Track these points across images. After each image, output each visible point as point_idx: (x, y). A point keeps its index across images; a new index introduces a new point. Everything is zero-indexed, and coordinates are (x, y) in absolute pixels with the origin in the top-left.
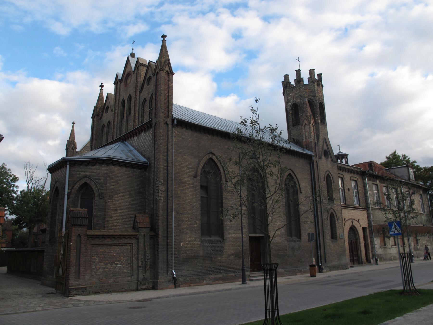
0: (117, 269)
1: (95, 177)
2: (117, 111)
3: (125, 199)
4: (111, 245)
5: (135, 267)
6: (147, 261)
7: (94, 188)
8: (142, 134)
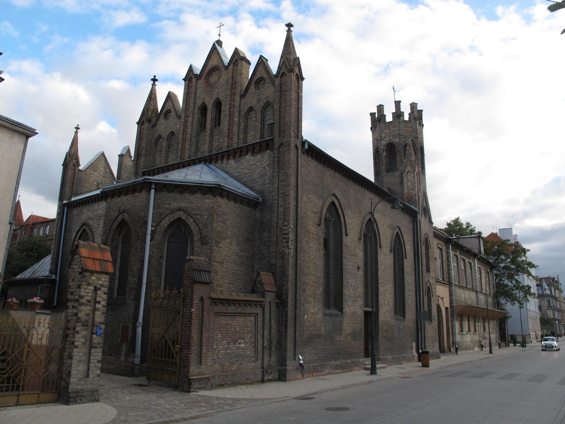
1: (195, 212)
2: (190, 119)
3: (232, 248)
4: (233, 315)
5: (260, 348)
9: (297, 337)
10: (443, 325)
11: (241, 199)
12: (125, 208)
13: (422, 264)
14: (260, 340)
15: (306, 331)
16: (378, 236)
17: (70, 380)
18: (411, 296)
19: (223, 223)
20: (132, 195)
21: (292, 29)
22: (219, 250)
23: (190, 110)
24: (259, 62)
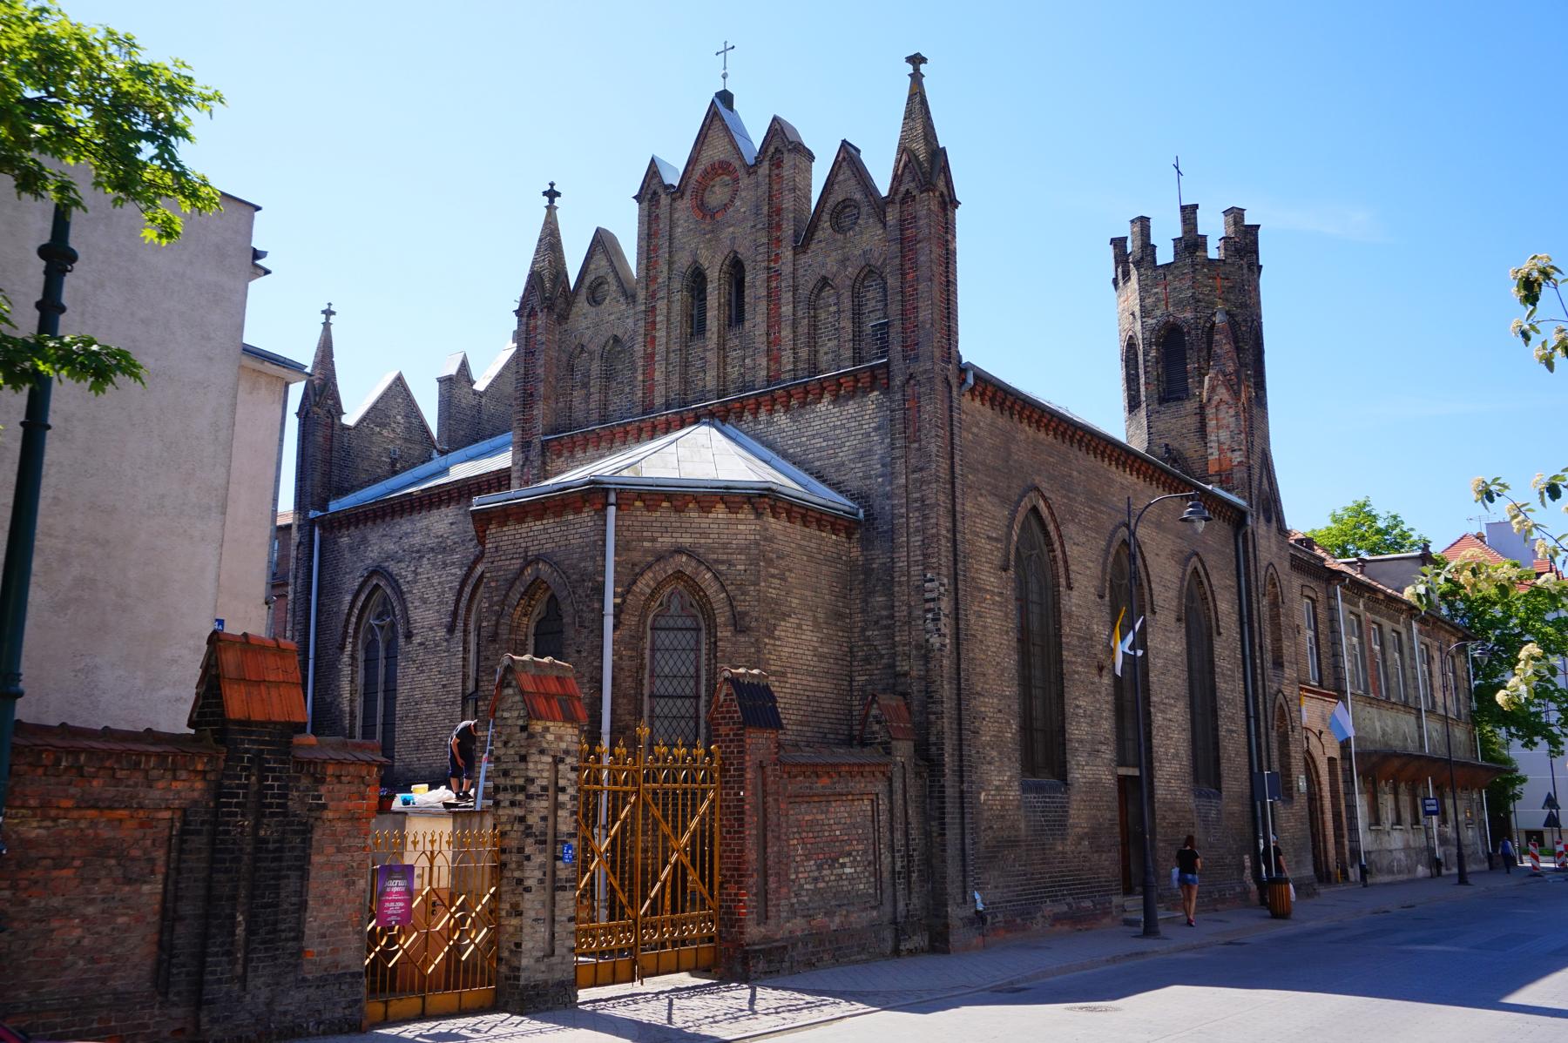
2: (661, 306)
3: (804, 637)
5: (886, 875)
9: (967, 847)
10: (1322, 805)
11: (818, 516)
12: (541, 552)
13: (1261, 647)
14: (886, 857)
15: (984, 831)
16: (1145, 584)
17: (520, 961)
19: (780, 579)
20: (557, 520)
22: (775, 645)
23: (660, 280)
24: (840, 159)
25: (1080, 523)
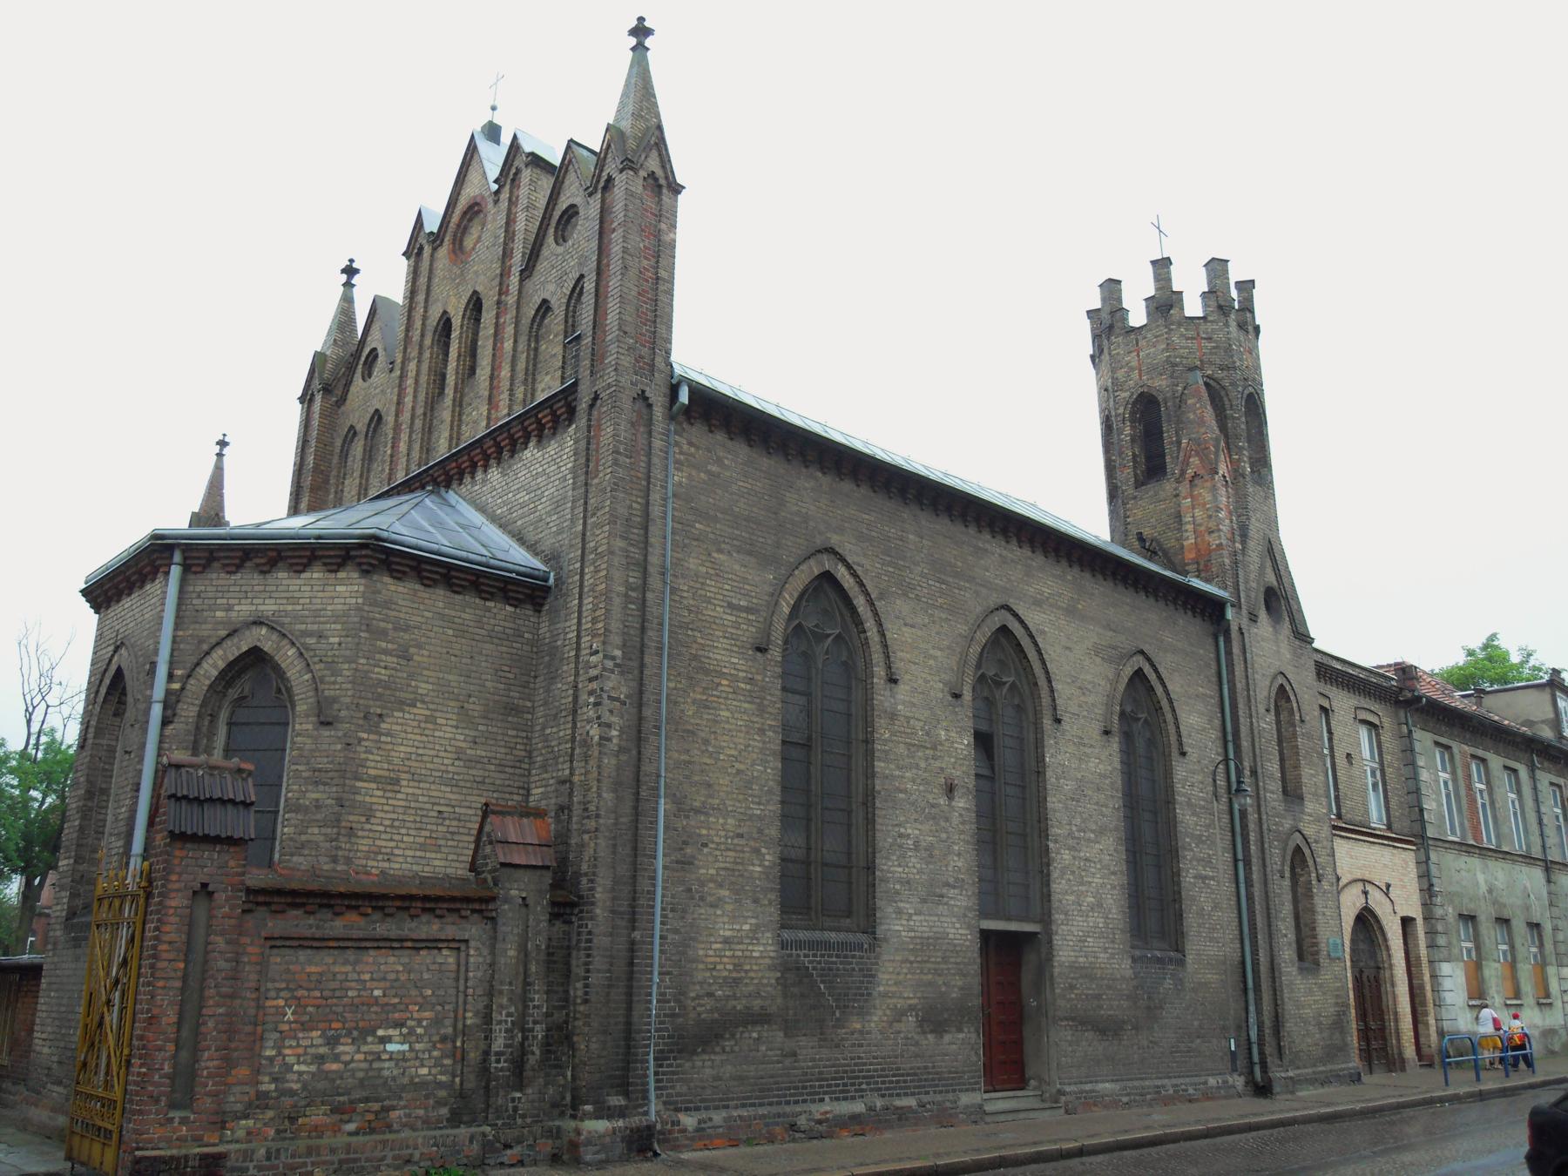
0: (387, 1065)
1: (303, 627)
2: (412, 366)
3: (437, 734)
4: (360, 944)
6: (532, 1030)
7: (292, 673)
8: (527, 454)
16: (1042, 682)
18: (1212, 878)
21: (648, 42)
25: (918, 598)
